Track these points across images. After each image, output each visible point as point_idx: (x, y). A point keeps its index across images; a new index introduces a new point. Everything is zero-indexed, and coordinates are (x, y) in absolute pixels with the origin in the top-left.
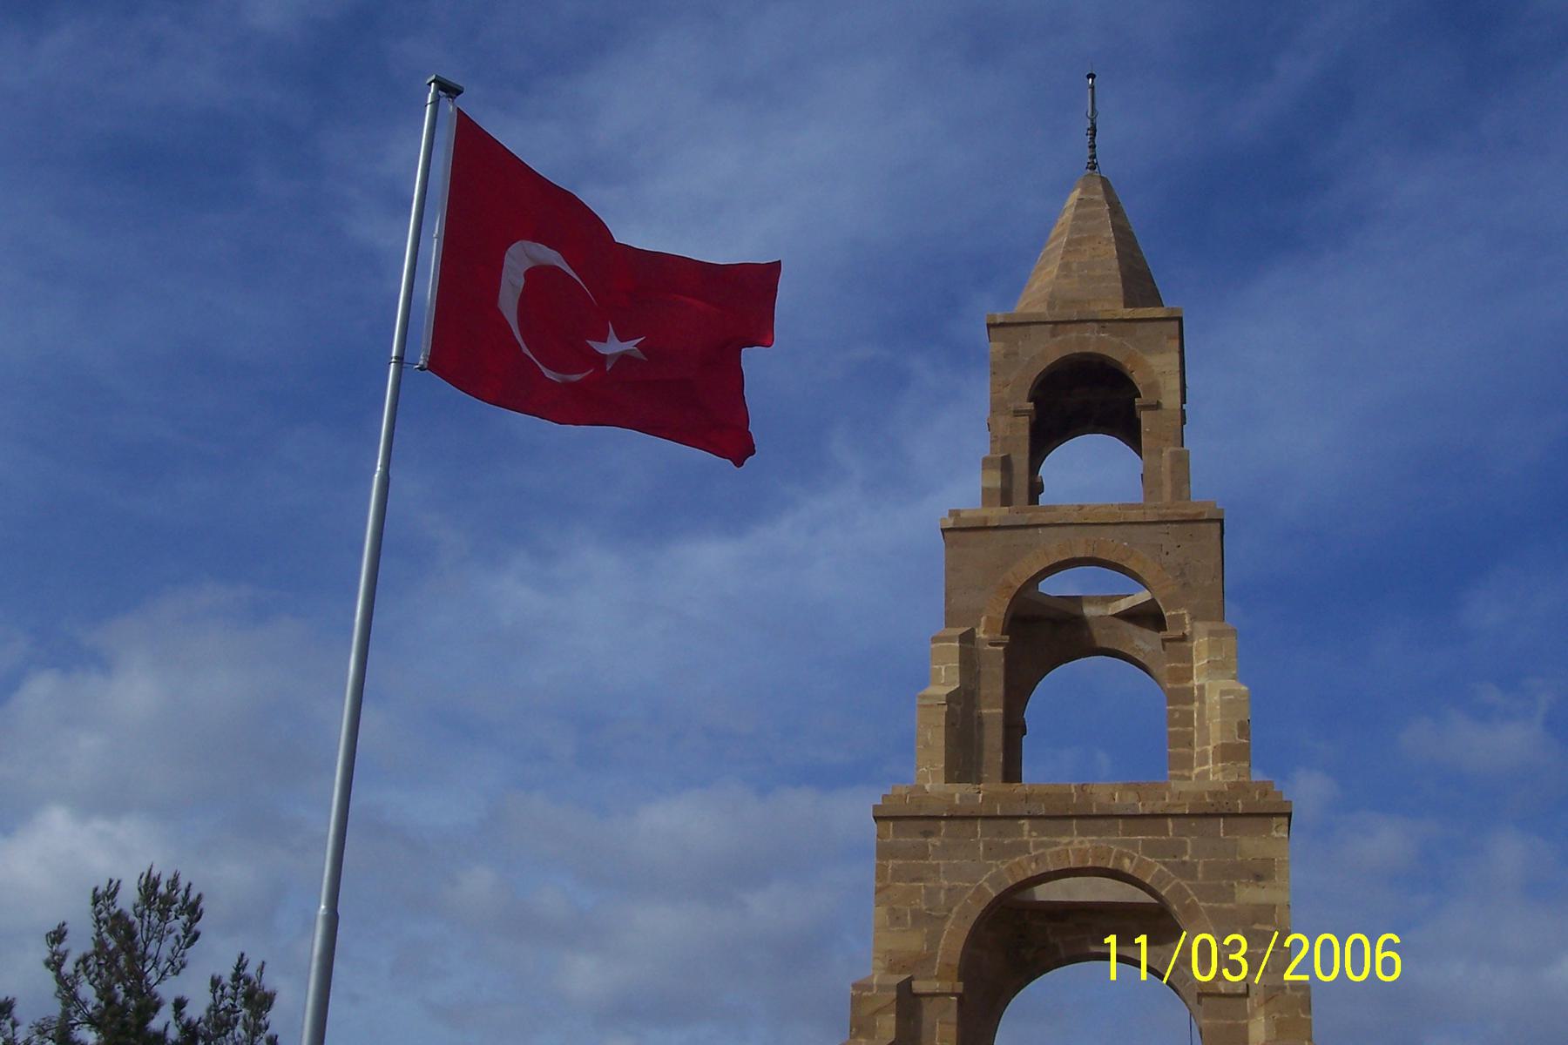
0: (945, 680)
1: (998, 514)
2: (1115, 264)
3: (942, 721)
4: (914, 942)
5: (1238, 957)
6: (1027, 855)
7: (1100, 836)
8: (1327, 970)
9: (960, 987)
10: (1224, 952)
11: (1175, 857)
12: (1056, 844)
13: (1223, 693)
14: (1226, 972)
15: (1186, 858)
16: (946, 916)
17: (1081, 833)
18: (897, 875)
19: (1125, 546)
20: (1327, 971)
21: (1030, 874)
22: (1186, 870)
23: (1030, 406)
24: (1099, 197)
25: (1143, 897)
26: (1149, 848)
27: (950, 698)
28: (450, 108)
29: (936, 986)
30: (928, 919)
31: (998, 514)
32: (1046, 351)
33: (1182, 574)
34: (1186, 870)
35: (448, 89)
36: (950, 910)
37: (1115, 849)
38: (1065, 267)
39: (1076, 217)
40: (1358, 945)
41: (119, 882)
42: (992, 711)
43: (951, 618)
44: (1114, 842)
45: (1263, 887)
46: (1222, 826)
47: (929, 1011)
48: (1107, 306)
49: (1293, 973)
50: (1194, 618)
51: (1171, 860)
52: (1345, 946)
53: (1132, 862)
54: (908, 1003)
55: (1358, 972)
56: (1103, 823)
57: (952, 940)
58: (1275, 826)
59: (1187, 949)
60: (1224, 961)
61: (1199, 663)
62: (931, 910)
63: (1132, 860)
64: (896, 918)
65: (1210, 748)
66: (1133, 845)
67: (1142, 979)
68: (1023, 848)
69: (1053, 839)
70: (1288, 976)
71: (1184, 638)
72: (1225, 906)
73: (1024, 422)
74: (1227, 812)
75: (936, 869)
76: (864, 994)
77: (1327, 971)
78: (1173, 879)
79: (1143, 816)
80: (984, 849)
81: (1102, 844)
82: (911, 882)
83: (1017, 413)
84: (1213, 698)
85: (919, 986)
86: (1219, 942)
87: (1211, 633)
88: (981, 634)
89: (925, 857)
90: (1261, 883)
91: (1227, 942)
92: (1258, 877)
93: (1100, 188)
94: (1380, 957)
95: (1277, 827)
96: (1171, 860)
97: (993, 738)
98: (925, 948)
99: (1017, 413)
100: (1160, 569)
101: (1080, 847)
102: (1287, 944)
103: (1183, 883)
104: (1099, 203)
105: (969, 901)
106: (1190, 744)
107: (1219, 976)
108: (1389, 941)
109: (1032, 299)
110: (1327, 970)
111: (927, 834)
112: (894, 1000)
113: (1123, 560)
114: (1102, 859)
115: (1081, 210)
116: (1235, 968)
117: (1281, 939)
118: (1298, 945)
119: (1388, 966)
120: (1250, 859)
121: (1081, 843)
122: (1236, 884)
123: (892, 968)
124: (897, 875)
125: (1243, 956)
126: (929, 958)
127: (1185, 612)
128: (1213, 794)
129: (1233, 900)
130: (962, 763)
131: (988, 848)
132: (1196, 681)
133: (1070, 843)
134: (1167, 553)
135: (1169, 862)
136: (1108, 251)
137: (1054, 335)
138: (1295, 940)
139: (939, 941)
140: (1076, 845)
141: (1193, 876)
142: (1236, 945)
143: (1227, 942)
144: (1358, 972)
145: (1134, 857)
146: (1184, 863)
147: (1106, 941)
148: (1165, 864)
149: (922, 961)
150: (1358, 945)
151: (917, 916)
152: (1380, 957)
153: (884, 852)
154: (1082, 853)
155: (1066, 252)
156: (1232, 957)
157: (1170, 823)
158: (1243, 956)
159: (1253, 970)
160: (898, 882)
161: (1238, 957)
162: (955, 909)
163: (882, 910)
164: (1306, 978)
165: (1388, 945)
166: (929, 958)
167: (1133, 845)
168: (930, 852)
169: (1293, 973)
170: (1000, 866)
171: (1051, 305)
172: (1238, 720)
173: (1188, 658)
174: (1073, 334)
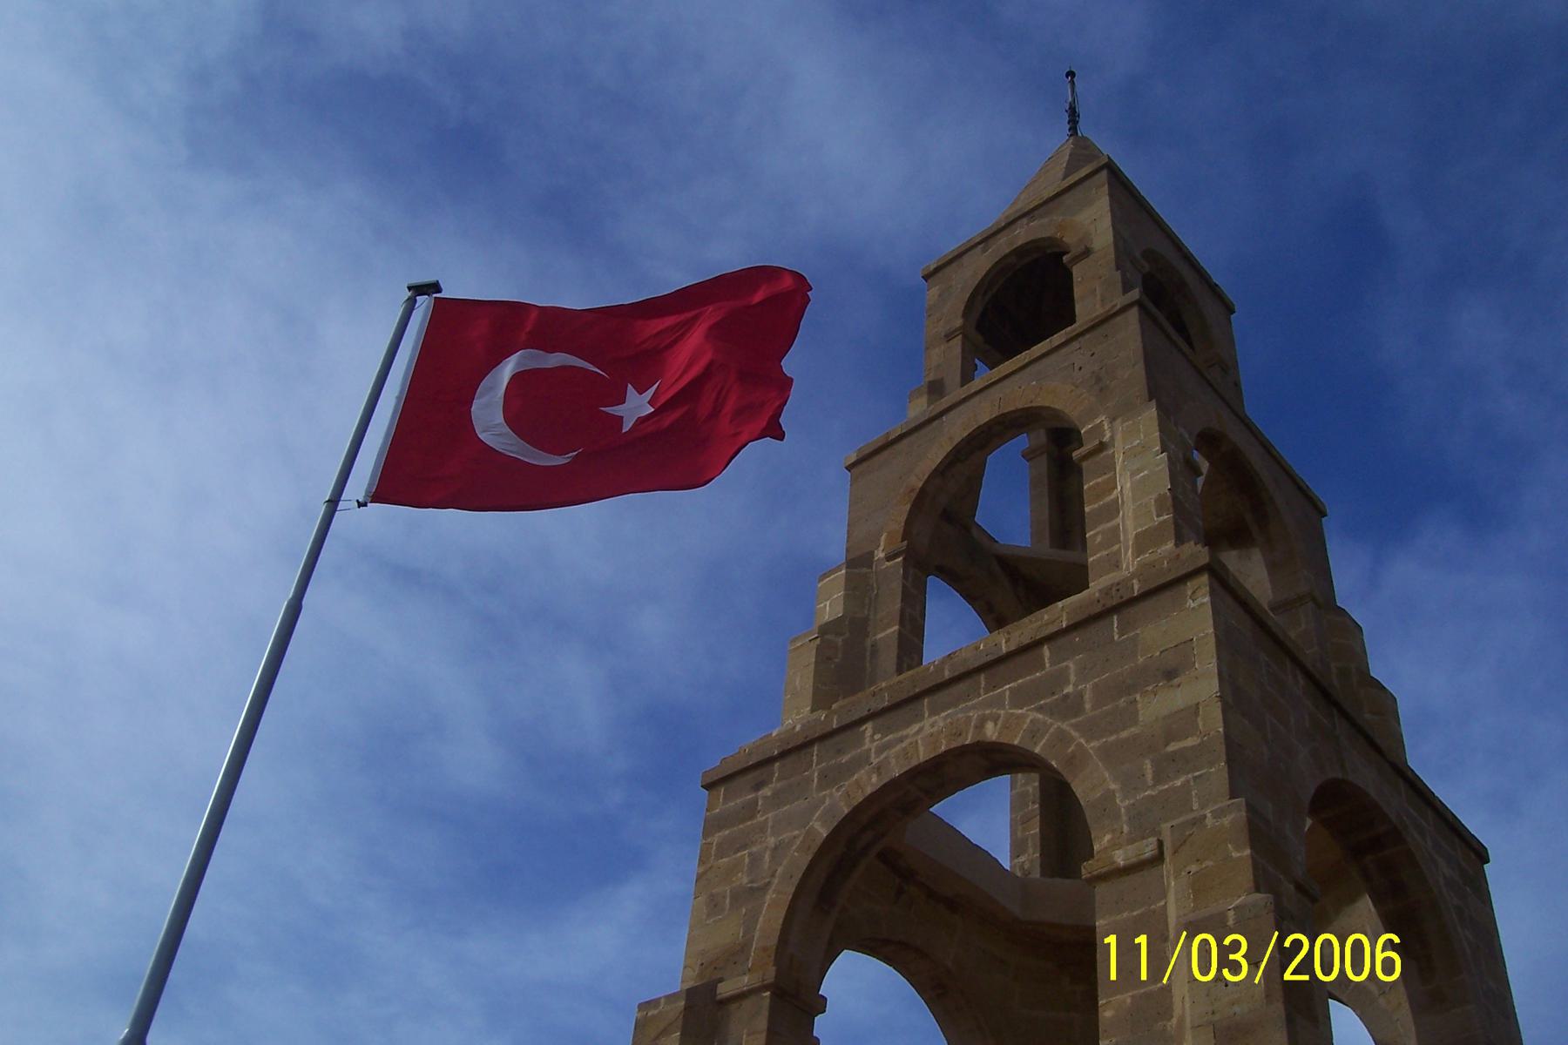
5: (1237, 957)
6: (867, 767)
7: (956, 706)
8: (1327, 970)
10: (1224, 952)
11: (1053, 694)
12: (901, 740)
14: (1225, 972)
15: (1069, 689)
16: (769, 882)
17: (933, 713)
19: (1034, 386)
20: (1327, 972)
21: (869, 790)
22: (1071, 707)
26: (1019, 698)
33: (1099, 379)
34: (1071, 707)
36: (773, 876)
37: (974, 715)
44: (974, 707)
45: (1179, 686)
46: (1116, 625)
50: (1113, 420)
51: (1048, 701)
52: (1345, 946)
53: (996, 724)
55: (1358, 972)
56: (962, 687)
58: (1189, 593)
60: (1224, 962)
62: (752, 882)
63: (996, 719)
68: (863, 760)
69: (900, 734)
71: (1102, 447)
72: (1124, 734)
74: (1120, 601)
75: (762, 828)
76: (650, 1014)
77: (1327, 972)
78: (1052, 724)
79: (1010, 656)
80: (819, 779)
81: (960, 715)
82: (735, 853)
90: (1176, 681)
91: (1227, 942)
92: (1170, 675)
94: (1380, 957)
95: (1194, 592)
96: (1048, 701)
98: (741, 934)
100: (1073, 388)
101: (932, 730)
102: (1287, 944)
103: (1065, 726)
105: (796, 854)
107: (1219, 977)
110: (1327, 970)
111: (758, 786)
112: (681, 1013)
113: (1031, 402)
114: (960, 735)
116: (1235, 968)
117: (1281, 940)
118: (1297, 945)
120: (1158, 653)
121: (932, 726)
122: (1138, 698)
125: (1243, 956)
126: (744, 948)
127: (1103, 418)
129: (1135, 722)
133: (921, 729)
134: (1080, 368)
135: (1046, 704)
138: (1301, 941)
139: (757, 920)
140: (928, 730)
142: (1236, 946)
143: (1227, 942)
144: (1358, 972)
145: (999, 716)
146: (1067, 696)
148: (1040, 709)
150: (1358, 945)
152: (1380, 957)
156: (1232, 957)
158: (1243, 956)
159: (1254, 965)
160: (722, 858)
161: (1237, 957)
162: (780, 870)
164: (1306, 978)
166: (744, 948)
167: (998, 701)
168: (759, 808)
172: (1154, 496)
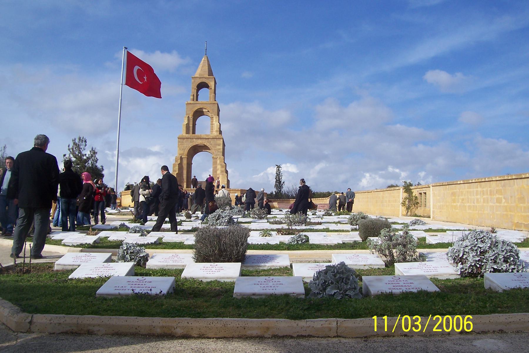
0: (186, 122)
1: (192, 102)
2: (207, 70)
3: (185, 127)
4: (182, 152)
5: (418, 323)
9: (187, 157)
10: (413, 321)
13: (217, 124)
14: (413, 328)
18: (180, 144)
22: (211, 144)
23: (196, 88)
24: (206, 60)
25: (262, 195)
26: (208, 142)
27: (186, 124)
28: (126, 51)
29: (184, 157)
30: (184, 150)
31: (192, 102)
32: (199, 81)
34: (211, 144)
35: (126, 48)
38: (201, 70)
39: (203, 62)
40: (458, 319)
41: (95, 148)
42: (191, 125)
43: (187, 115)
47: (184, 159)
48: (206, 76)
49: (436, 329)
52: (462, 327)
54: (181, 158)
57: (186, 152)
59: (400, 320)
61: (214, 121)
64: (180, 149)
65: (215, 130)
66: (205, 141)
67: (385, 331)
70: (434, 330)
73: (196, 90)
83: (195, 89)
84: (215, 125)
85: (182, 157)
86: (411, 319)
87: (216, 117)
88: (190, 116)
89: (183, 142)
92: (219, 145)
93: (206, 58)
94: (465, 323)
97: (191, 129)
99: (195, 89)
102: (434, 319)
104: (206, 60)
106: (213, 130)
108: (468, 318)
109: (197, 75)
115: (204, 61)
116: (417, 327)
119: (468, 326)
123: (180, 155)
124: (180, 144)
125: (419, 323)
128: (215, 136)
130: (188, 132)
131: (190, 142)
132: (214, 123)
136: (206, 68)
137: (200, 79)
141: (212, 145)
142: (417, 320)
147: (373, 318)
149: (183, 154)
151: (182, 149)
152: (465, 323)
153: (179, 142)
154: (200, 142)
155: (202, 68)
156: (416, 323)
157: (210, 139)
158: (419, 323)
161: (418, 323)
163: (179, 148)
164: (441, 330)
165: (468, 319)
169: (436, 329)
170: (191, 144)
171: (199, 75)
173: (213, 120)
174: (202, 79)
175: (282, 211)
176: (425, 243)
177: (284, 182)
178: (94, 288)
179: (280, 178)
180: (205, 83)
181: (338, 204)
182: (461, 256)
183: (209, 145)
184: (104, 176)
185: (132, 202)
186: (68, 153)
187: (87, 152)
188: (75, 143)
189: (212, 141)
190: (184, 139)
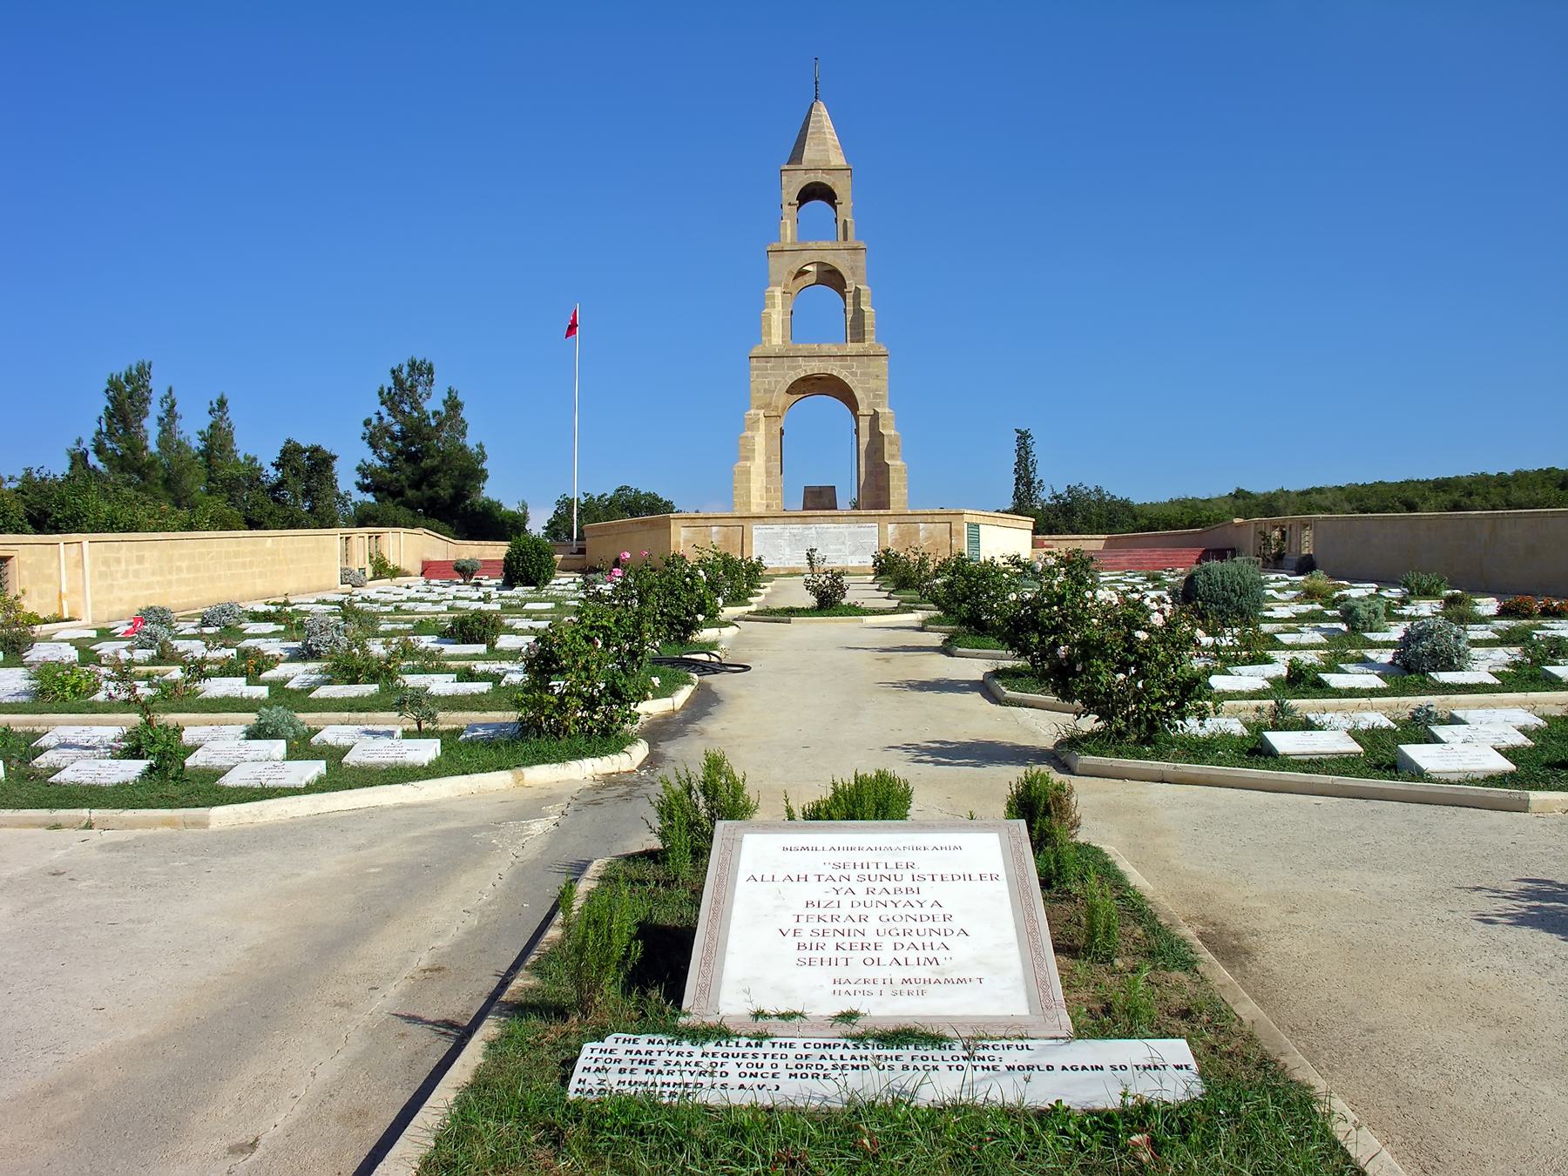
26: (842, 367)
34: (854, 374)
66: (836, 366)
137: (806, 174)
175: (1493, 674)
176: (460, 495)
177: (1041, 480)
178: (1185, 1107)
179: (1031, 469)
180: (823, 184)
181: (1456, 591)
182: (1333, 684)
183: (847, 377)
184: (487, 477)
185: (1437, 740)
186: (134, 367)
187: (433, 404)
188: (398, 381)
189: (855, 364)
190: (768, 359)
